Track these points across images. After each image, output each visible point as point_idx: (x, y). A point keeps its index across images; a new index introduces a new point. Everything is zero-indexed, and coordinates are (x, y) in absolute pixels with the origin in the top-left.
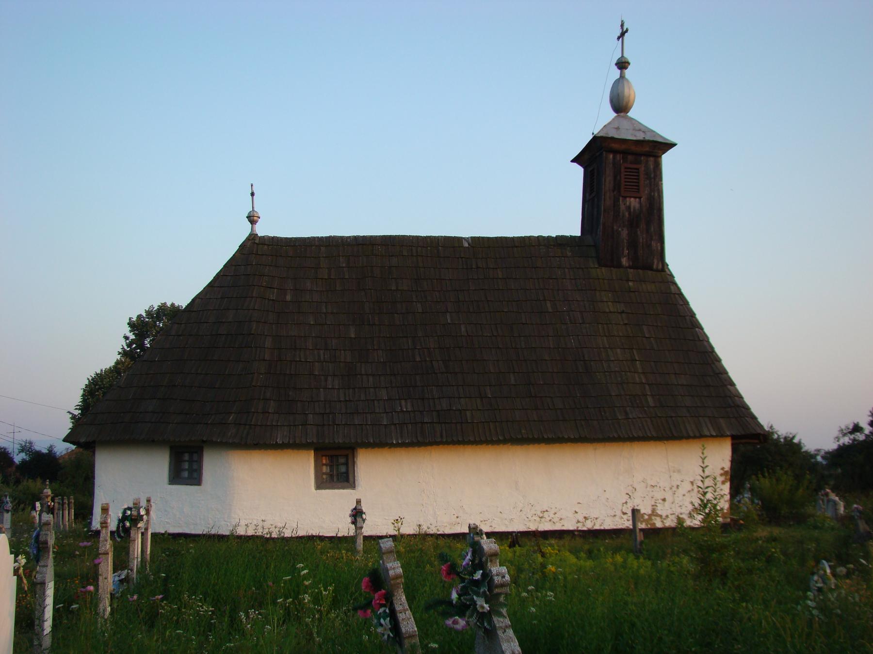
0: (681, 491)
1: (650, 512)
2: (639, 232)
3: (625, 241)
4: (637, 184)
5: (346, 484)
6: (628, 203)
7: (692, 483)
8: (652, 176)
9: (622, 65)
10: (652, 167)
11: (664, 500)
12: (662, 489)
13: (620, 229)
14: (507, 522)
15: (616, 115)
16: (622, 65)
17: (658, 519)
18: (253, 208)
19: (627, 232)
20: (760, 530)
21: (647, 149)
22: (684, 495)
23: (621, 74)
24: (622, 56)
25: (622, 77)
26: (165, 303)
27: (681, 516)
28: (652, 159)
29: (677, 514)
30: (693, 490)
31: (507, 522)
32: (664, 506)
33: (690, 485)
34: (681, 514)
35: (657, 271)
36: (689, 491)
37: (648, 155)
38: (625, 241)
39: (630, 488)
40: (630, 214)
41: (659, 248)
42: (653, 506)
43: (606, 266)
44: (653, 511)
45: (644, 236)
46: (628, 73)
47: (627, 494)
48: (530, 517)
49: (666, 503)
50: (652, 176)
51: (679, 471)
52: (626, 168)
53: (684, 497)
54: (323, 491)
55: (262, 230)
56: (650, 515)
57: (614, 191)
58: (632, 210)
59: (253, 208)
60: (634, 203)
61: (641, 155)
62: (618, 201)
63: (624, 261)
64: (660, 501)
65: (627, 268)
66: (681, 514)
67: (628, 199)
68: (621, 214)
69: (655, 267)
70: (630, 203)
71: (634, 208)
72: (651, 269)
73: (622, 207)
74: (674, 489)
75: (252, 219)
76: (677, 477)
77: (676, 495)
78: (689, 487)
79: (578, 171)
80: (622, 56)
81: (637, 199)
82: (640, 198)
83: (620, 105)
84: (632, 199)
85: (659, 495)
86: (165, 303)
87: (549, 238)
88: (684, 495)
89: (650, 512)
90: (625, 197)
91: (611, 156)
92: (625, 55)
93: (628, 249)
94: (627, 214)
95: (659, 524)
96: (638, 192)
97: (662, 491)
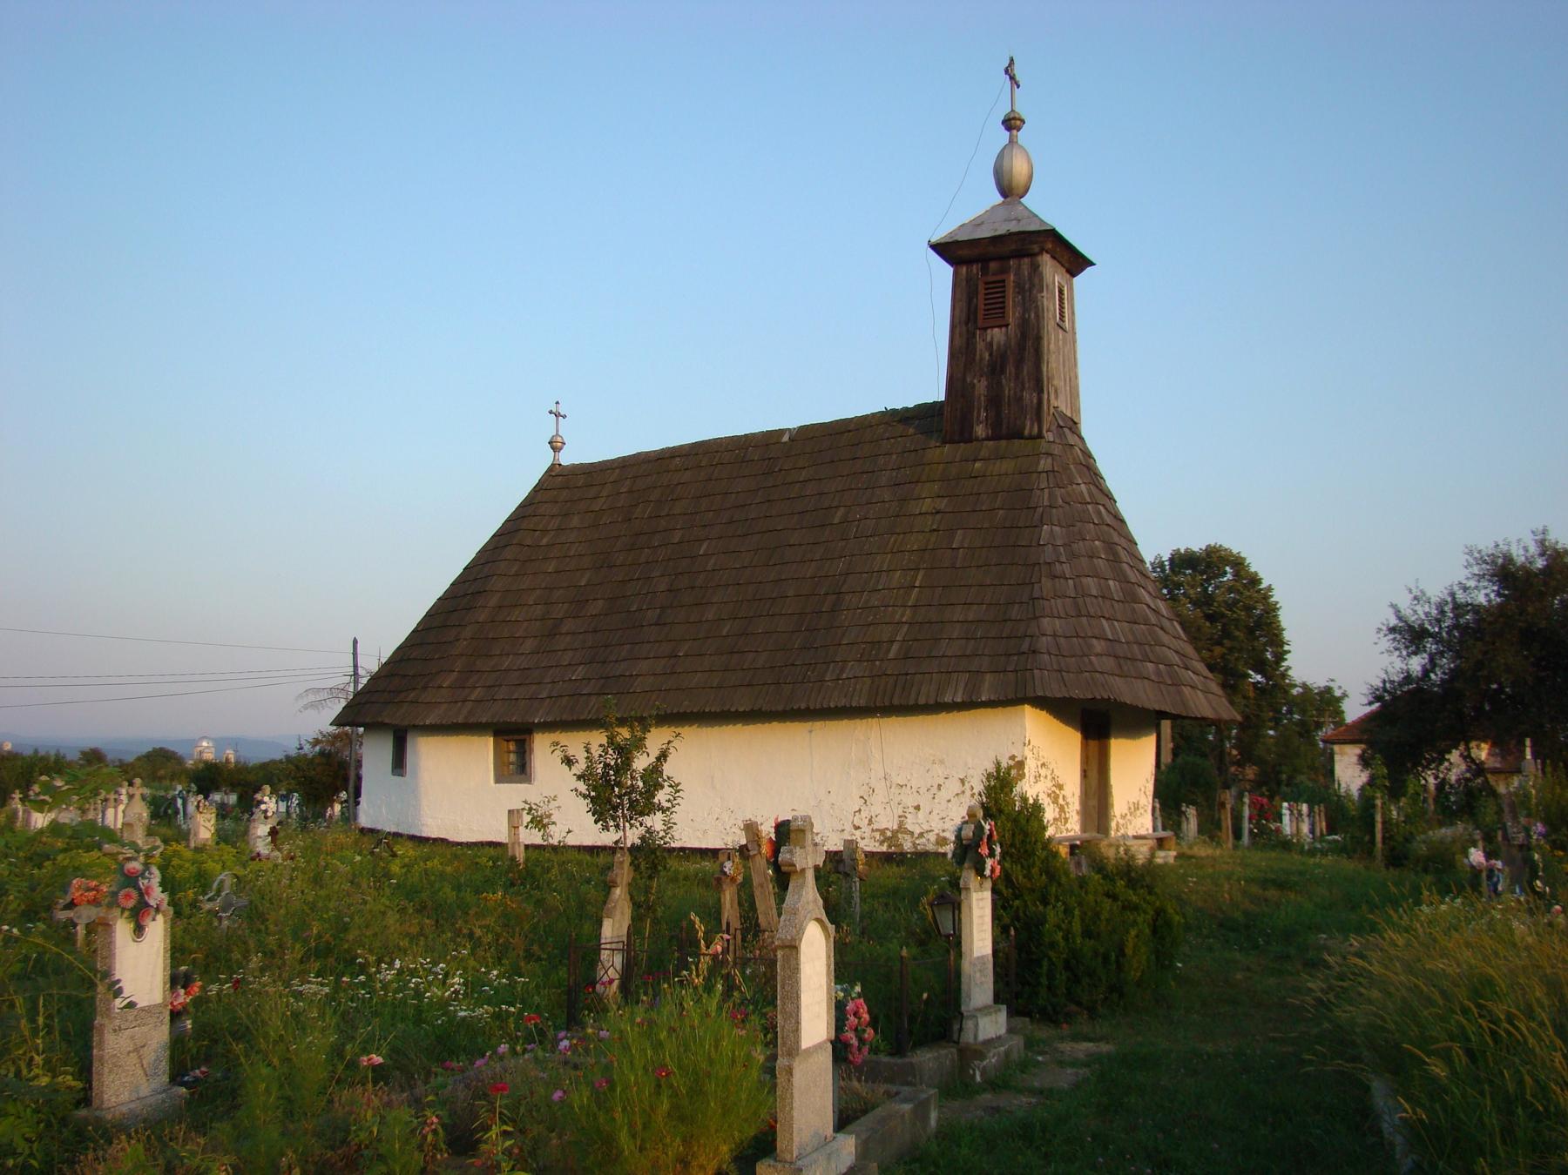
0: (944, 794)
1: (895, 827)
2: (1004, 381)
3: (982, 398)
4: (1001, 305)
5: (523, 776)
6: (989, 339)
7: (962, 781)
8: (1027, 286)
9: (1012, 123)
10: (1026, 273)
11: (917, 808)
12: (914, 790)
13: (975, 381)
14: (699, 834)
15: (1000, 199)
16: (1012, 123)
17: (908, 837)
18: (557, 431)
19: (986, 383)
20: (1171, 861)
21: (1013, 247)
22: (949, 801)
23: (1010, 136)
24: (1012, 110)
25: (1012, 142)
26: (1179, 549)
27: (942, 834)
28: (1026, 260)
29: (936, 831)
30: (963, 792)
31: (699, 834)
32: (917, 817)
33: (959, 784)
34: (944, 831)
35: (1031, 438)
36: (957, 795)
37: (1019, 255)
38: (982, 398)
39: (866, 787)
40: (991, 355)
41: (1035, 401)
42: (900, 817)
43: (952, 442)
44: (901, 825)
45: (1012, 384)
46: (1022, 136)
47: (862, 797)
48: (728, 828)
49: (921, 814)
50: (1027, 286)
51: (942, 762)
52: (986, 283)
53: (950, 804)
54: (502, 785)
55: (568, 458)
56: (895, 833)
57: (967, 324)
58: (995, 347)
59: (557, 431)
60: (997, 335)
61: (1009, 258)
62: (974, 335)
63: (980, 431)
64: (911, 810)
65: (983, 440)
66: (944, 831)
67: (989, 331)
68: (978, 357)
69: (1026, 432)
70: (992, 338)
71: (999, 343)
72: (1020, 436)
73: (980, 345)
74: (934, 790)
75: (555, 446)
76: (939, 771)
77: (936, 801)
78: (957, 787)
79: (944, 273)
80: (557, 435)
81: (1004, 329)
82: (1007, 326)
83: (1009, 190)
84: (996, 330)
85: (910, 801)
86: (1179, 549)
87: (906, 410)
88: (949, 801)
89: (895, 827)
90: (985, 329)
91: (964, 269)
92: (1017, 109)
93: (986, 410)
94: (987, 356)
95: (907, 846)
96: (1004, 317)
97: (915, 793)
